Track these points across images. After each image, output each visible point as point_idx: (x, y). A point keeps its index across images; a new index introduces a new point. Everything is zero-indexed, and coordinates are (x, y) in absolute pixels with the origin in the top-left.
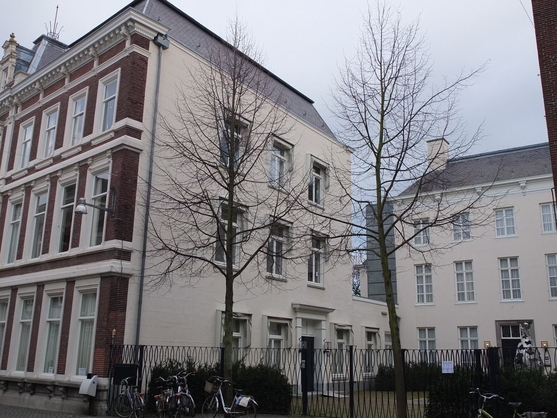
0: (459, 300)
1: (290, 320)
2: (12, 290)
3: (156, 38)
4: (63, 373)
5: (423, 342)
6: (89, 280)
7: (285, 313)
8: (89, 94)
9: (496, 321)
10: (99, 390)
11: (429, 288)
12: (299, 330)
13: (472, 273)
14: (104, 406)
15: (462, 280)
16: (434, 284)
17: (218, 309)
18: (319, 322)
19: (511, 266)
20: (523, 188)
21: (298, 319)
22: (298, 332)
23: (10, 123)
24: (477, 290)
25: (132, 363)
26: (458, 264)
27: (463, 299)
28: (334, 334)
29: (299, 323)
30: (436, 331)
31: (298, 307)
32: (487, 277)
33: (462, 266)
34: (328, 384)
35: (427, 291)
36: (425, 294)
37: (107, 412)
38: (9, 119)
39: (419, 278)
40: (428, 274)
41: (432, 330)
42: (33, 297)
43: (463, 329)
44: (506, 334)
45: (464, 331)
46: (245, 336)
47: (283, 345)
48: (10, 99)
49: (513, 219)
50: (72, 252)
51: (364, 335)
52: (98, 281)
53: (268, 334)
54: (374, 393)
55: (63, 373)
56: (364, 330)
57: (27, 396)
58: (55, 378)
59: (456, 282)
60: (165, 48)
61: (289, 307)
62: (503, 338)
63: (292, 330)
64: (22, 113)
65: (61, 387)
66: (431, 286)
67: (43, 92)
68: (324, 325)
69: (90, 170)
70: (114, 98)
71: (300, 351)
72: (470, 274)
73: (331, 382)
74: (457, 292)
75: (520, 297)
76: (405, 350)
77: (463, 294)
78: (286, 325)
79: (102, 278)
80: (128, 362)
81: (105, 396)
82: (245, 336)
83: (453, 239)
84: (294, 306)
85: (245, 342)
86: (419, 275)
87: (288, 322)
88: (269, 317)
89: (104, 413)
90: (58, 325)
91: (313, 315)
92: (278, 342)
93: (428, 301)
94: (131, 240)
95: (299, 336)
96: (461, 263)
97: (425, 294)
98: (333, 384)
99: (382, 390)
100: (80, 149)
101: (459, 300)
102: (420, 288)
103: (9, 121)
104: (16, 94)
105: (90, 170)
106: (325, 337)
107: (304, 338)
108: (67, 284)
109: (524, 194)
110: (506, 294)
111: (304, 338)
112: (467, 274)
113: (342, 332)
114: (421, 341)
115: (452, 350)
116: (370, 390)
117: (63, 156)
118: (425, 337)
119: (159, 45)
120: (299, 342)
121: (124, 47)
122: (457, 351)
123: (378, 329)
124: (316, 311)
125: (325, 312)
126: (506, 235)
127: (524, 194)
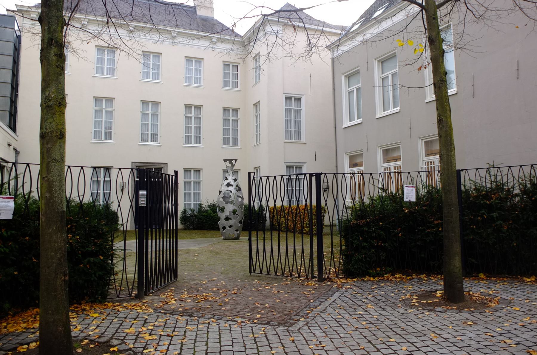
0: (94, 138)
9: (133, 162)
19: (106, 106)
20: (131, 31)
25: (285, 204)
27: (228, 144)
33: (191, 110)
54: (292, 235)
58: (326, 226)
75: (111, 139)
80: (279, 204)
83: (95, 72)
93: (106, 138)
96: (191, 107)
101: (94, 138)
109: (173, 44)
110: (188, 139)
112: (106, 112)
126: (151, 80)
127: (173, 44)
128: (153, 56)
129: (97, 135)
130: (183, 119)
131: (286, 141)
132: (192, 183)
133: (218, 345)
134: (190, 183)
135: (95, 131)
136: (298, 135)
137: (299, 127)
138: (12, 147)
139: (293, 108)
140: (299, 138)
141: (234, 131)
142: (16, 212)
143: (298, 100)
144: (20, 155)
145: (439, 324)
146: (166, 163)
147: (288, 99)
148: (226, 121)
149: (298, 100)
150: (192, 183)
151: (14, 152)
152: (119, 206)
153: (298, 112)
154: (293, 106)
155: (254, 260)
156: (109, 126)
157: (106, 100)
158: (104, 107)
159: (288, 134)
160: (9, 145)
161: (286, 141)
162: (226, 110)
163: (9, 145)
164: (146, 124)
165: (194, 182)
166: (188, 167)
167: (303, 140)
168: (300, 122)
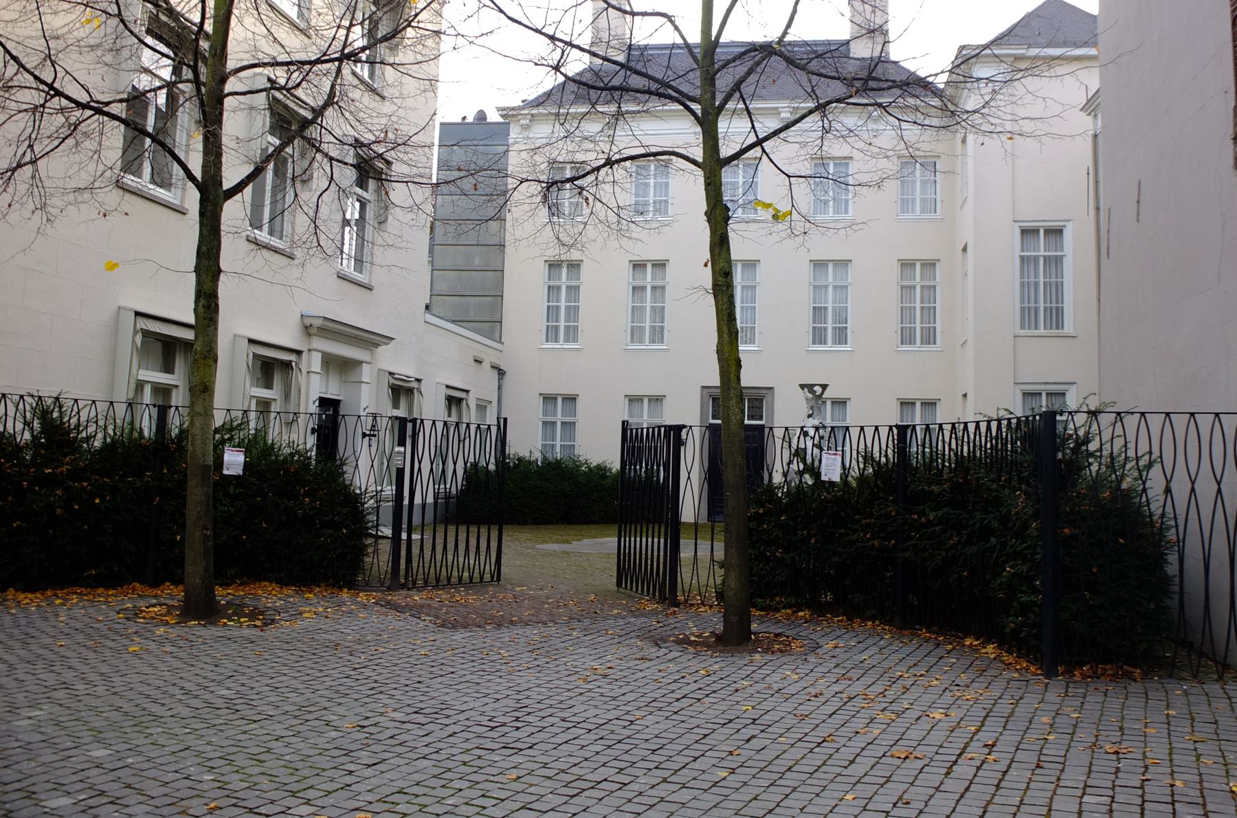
0: (632, 341)
1: (298, 353)
5: (548, 425)
7: (285, 335)
11: (573, 312)
12: (315, 379)
13: (663, 288)
15: (643, 300)
16: (584, 304)
17: (122, 304)
18: (356, 364)
21: (314, 353)
22: (313, 385)
24: (583, 323)
26: (638, 266)
28: (386, 393)
29: (316, 363)
30: (580, 403)
31: (318, 323)
32: (873, 304)
34: (424, 505)
35: (567, 320)
36: (562, 324)
39: (553, 290)
40: (659, 283)
41: (571, 399)
45: (636, 405)
49: (667, 184)
51: (442, 402)
53: (248, 384)
56: (443, 392)
59: (631, 305)
61: (294, 322)
62: (747, 422)
63: (299, 379)
66: (576, 308)
68: (366, 373)
71: (313, 431)
72: (659, 290)
73: (430, 500)
74: (630, 324)
76: (684, 427)
77: (642, 329)
78: (287, 365)
82: (287, 396)
84: (308, 322)
86: (552, 283)
87: (292, 357)
88: (251, 341)
91: (347, 343)
95: (315, 395)
97: (562, 322)
98: (436, 503)
99: (468, 522)
101: (632, 341)
102: (552, 312)
106: (367, 398)
107: (324, 403)
110: (907, 337)
111: (324, 403)
112: (654, 288)
113: (401, 391)
114: (545, 423)
115: (877, 428)
116: (446, 522)
118: (555, 415)
120: (314, 408)
123: (467, 392)
124: (356, 338)
125: (370, 340)
128: (835, 164)
129: (636, 334)
130: (896, 292)
131: (1023, 332)
132: (559, 424)
133: (1210, 807)
134: (554, 423)
135: (633, 328)
136: (1056, 317)
137: (1059, 298)
138: (486, 365)
139: (1042, 253)
140: (1059, 324)
141: (925, 312)
142: (246, 466)
143: (1055, 233)
144: (507, 378)
145: (161, 683)
146: (772, 388)
147: (1028, 233)
148: (907, 290)
149: (1055, 233)
150: (559, 424)
151: (496, 372)
152: (1193, 490)
153: (1055, 262)
154: (1041, 249)
155: (415, 565)
156: (841, 316)
157: (743, 266)
158: (649, 280)
159: (1028, 316)
160: (478, 361)
161: (1023, 332)
162: (907, 265)
163: (478, 361)
164: (820, 308)
165: (563, 423)
166: (909, 395)
167: (1068, 328)
168: (1059, 286)
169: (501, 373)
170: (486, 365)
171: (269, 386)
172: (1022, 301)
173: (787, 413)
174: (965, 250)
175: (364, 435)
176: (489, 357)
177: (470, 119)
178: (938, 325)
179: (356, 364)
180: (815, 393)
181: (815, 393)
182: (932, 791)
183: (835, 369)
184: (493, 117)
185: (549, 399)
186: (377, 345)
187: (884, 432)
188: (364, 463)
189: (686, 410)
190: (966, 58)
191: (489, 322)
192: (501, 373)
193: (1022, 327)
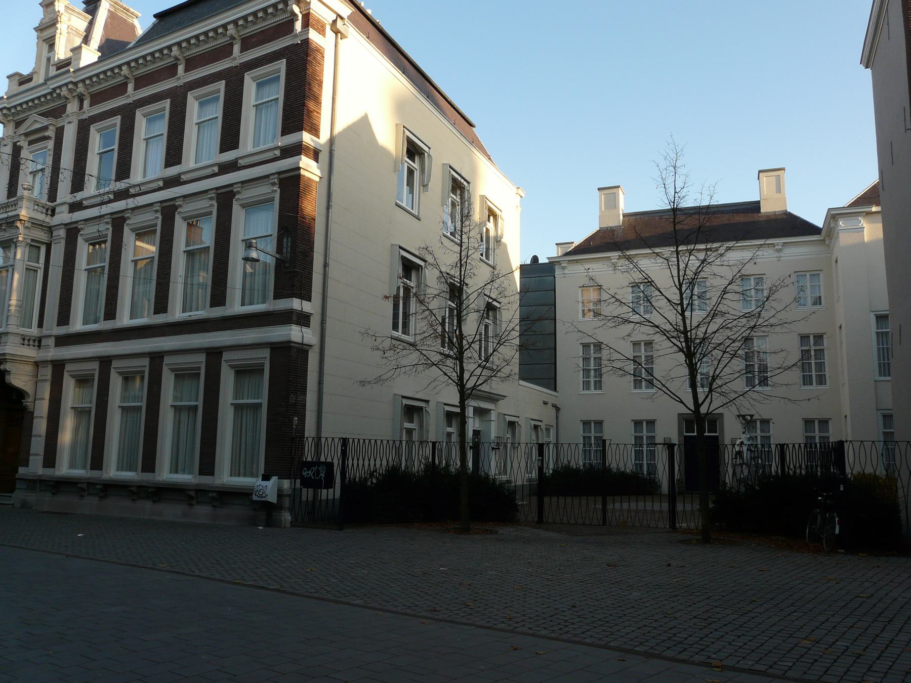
2: (151, 358)
3: (335, 22)
4: (212, 473)
6: (258, 351)
8: (121, 125)
10: (280, 495)
14: (287, 517)
23: (70, 123)
37: (291, 522)
38: (68, 116)
42: (93, 375)
43: (638, 423)
44: (689, 429)
46: (421, 426)
47: (415, 437)
48: (70, 86)
50: (160, 319)
52: (266, 353)
55: (212, 473)
57: (148, 505)
60: (343, 37)
64: (89, 111)
65: (214, 492)
67: (89, 99)
68: (493, 416)
69: (128, 225)
70: (113, 150)
78: (420, 409)
79: (272, 349)
81: (287, 502)
82: (421, 426)
85: (421, 435)
89: (288, 525)
90: (90, 412)
92: (410, 432)
94: (309, 300)
100: (161, 184)
103: (69, 119)
104: (83, 81)
105: (128, 225)
108: (207, 356)
117: (241, 162)
118: (590, 432)
119: (337, 32)
121: (65, 112)
122: (800, 446)
131: (883, 378)
144: (561, 412)
160: (545, 403)
163: (545, 403)
166: (810, 416)
169: (558, 409)
170: (550, 405)
171: (411, 421)
172: (879, 360)
173: (732, 431)
174: (840, 327)
175: (493, 449)
176: (551, 401)
177: (529, 262)
178: (827, 373)
179: (487, 411)
180: (749, 422)
181: (749, 422)
182: (851, 669)
183: (759, 404)
184: (543, 260)
185: (586, 423)
186: (498, 400)
187: (336, 440)
188: (493, 464)
189: (669, 429)
190: (833, 216)
191: (551, 382)
192: (558, 409)
193: (880, 375)
